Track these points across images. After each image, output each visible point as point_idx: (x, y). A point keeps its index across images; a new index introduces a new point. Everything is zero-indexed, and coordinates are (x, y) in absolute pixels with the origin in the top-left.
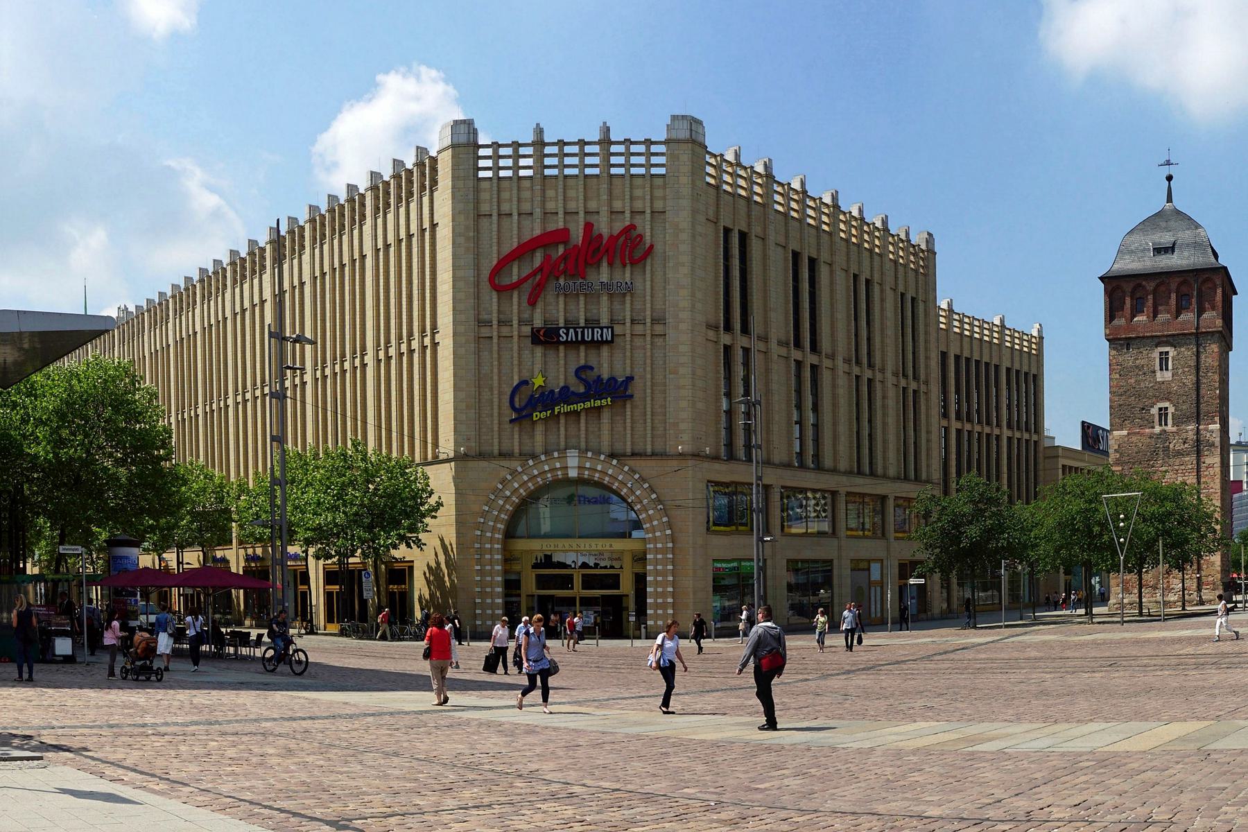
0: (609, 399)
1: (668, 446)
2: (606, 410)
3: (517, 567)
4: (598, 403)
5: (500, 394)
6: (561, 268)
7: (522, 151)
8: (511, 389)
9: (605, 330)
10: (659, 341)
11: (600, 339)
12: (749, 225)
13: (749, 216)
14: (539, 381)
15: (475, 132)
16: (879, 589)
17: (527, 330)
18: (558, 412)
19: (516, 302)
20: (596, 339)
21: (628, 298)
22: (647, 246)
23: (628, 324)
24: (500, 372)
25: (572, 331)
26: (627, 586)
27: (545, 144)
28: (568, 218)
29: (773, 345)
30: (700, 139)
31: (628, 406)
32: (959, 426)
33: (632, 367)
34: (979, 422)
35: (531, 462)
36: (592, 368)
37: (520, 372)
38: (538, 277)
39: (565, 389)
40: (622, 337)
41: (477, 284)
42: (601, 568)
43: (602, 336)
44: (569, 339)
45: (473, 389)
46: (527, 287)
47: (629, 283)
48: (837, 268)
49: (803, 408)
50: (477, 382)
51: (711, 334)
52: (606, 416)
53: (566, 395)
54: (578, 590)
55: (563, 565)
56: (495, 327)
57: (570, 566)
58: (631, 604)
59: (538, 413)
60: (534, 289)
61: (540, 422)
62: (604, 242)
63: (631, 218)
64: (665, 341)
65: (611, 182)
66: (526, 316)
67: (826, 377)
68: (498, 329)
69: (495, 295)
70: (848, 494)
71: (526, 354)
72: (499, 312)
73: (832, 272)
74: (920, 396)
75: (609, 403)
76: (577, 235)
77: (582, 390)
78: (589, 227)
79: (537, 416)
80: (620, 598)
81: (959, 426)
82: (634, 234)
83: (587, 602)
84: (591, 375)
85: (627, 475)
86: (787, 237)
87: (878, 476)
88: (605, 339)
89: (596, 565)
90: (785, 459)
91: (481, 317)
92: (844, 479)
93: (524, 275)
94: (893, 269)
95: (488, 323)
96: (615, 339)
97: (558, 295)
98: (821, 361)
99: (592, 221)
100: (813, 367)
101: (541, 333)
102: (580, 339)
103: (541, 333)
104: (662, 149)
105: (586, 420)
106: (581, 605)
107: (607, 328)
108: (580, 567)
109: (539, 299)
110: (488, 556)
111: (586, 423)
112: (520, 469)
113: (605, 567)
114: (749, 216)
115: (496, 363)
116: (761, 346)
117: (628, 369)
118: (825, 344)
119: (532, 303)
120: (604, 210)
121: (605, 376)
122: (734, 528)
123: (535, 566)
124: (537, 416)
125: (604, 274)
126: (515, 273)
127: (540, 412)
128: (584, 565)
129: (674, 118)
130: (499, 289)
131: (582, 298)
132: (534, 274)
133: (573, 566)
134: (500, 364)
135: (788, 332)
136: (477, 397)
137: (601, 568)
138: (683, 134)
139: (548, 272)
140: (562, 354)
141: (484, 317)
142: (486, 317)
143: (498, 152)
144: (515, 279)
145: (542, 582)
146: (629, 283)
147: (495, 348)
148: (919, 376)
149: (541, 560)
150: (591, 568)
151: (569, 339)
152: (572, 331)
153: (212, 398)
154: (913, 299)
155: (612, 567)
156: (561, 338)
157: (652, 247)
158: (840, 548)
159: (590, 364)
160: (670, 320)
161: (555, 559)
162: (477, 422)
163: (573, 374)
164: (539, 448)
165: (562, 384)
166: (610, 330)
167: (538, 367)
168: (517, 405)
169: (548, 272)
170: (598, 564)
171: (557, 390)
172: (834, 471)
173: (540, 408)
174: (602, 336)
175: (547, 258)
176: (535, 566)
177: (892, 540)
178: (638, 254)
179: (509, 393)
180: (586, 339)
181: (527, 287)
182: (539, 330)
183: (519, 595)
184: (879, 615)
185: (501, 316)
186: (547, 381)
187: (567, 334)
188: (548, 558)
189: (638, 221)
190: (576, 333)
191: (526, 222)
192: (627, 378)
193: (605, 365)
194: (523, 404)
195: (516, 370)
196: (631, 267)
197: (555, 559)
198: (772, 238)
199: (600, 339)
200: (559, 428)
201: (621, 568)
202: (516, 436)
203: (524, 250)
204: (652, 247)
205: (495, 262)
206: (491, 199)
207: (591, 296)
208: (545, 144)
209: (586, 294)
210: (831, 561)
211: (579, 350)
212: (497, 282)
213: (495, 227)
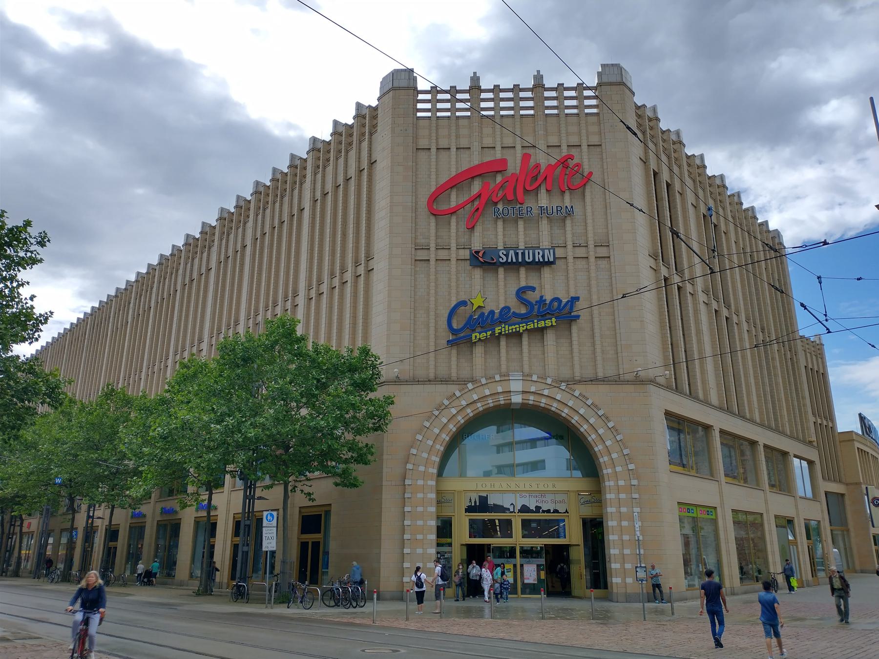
0: (554, 320)
2: (549, 331)
3: (447, 513)
4: (542, 324)
5: (437, 316)
8: (448, 311)
9: (546, 252)
11: (541, 260)
14: (477, 302)
15: (415, 79)
17: (466, 254)
18: (500, 333)
19: (455, 227)
20: (537, 260)
24: (436, 293)
25: (512, 252)
26: (573, 535)
31: (574, 329)
37: (458, 293)
38: (476, 203)
41: (415, 210)
42: (544, 512)
43: (543, 256)
44: (509, 260)
45: (408, 332)
52: (550, 337)
53: (506, 316)
54: (518, 539)
57: (509, 509)
58: (578, 555)
59: (477, 334)
60: (473, 214)
62: (542, 171)
66: (462, 240)
69: (433, 220)
72: (437, 237)
75: (554, 324)
76: (514, 166)
77: (523, 310)
78: (526, 157)
79: (476, 336)
80: (566, 547)
83: (528, 553)
84: (532, 297)
89: (538, 509)
91: (418, 241)
96: (557, 262)
101: (480, 254)
102: (520, 260)
103: (480, 254)
107: (549, 249)
108: (520, 511)
109: (478, 224)
110: (422, 468)
113: (548, 511)
115: (433, 284)
119: (471, 228)
120: (542, 145)
121: (548, 298)
123: (469, 509)
124: (476, 336)
125: (543, 200)
126: (454, 199)
127: (480, 333)
128: (525, 509)
130: (435, 214)
131: (521, 224)
132: (472, 200)
133: (512, 510)
134: (436, 287)
136: (412, 318)
137: (544, 512)
140: (501, 283)
141: (421, 241)
142: (423, 241)
144: (453, 204)
145: (479, 528)
147: (433, 270)
149: (475, 502)
150: (532, 511)
151: (509, 260)
152: (512, 252)
153: (154, 362)
155: (556, 511)
156: (501, 260)
157: (591, 174)
161: (491, 502)
164: (478, 372)
165: (502, 305)
166: (552, 251)
168: (455, 326)
170: (540, 508)
171: (497, 311)
174: (543, 256)
175: (486, 186)
176: (469, 509)
177: (798, 498)
179: (447, 315)
180: (527, 259)
182: (477, 252)
183: (450, 545)
185: (439, 241)
188: (484, 500)
190: (517, 254)
191: (465, 155)
194: (460, 326)
195: (454, 291)
196: (571, 194)
199: (541, 260)
201: (566, 512)
205: (433, 189)
206: (430, 135)
207: (531, 220)
211: (453, 492)
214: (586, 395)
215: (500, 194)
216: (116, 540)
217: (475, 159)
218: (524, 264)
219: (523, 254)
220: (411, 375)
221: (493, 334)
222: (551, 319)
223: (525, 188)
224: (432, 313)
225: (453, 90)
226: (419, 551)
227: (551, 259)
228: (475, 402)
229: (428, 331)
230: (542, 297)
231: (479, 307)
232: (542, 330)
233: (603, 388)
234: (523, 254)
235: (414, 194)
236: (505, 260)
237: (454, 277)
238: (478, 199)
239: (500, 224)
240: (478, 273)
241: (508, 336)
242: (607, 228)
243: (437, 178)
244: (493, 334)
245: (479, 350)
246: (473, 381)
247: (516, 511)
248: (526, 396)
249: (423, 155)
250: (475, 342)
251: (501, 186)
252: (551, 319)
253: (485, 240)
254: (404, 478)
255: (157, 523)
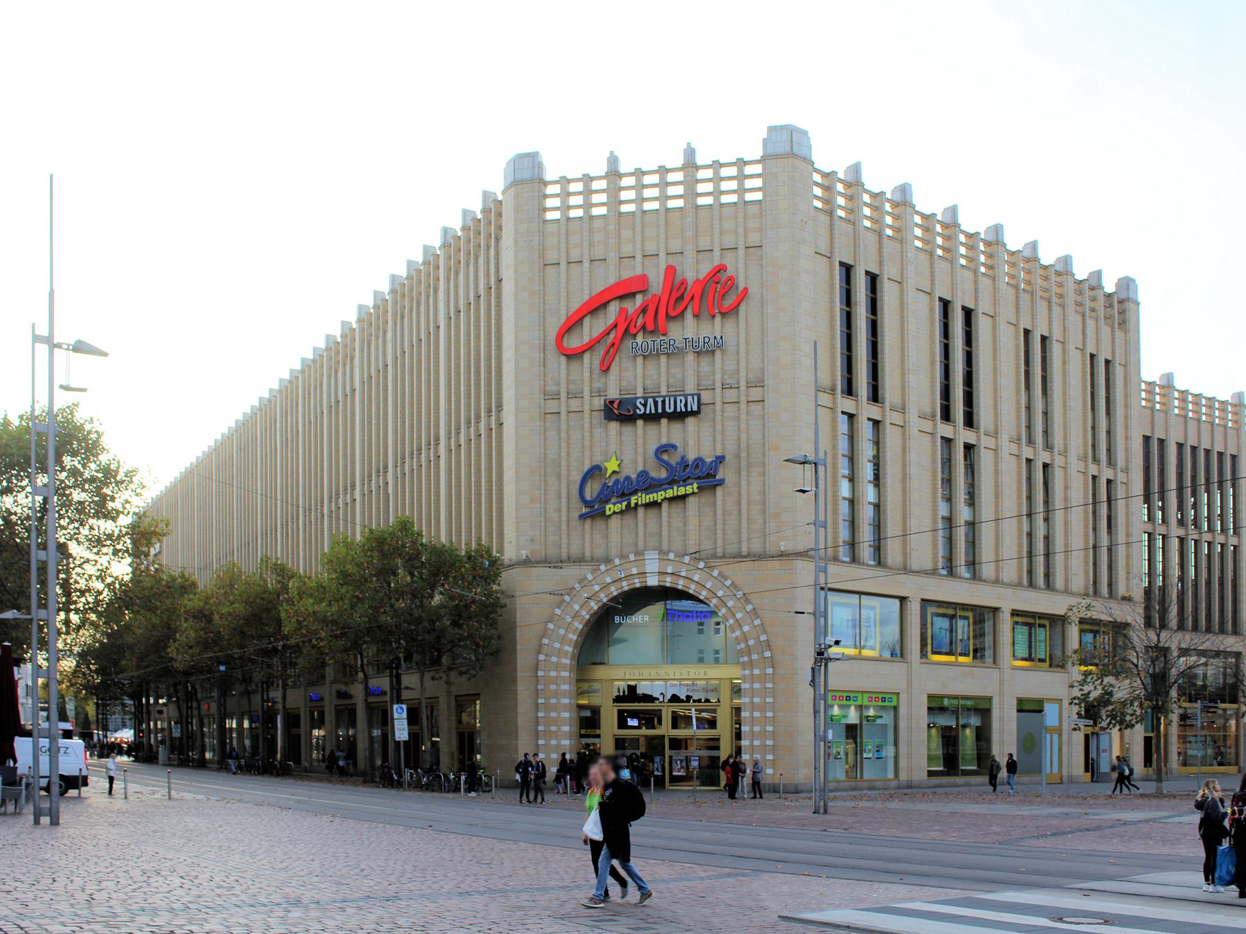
0: (695, 485)
1: (767, 544)
3: (595, 700)
4: (682, 491)
6: (639, 323)
7: (749, 170)
9: (690, 398)
10: (756, 409)
11: (684, 410)
12: (881, 264)
13: (880, 253)
14: (612, 466)
16: (1056, 737)
17: (599, 403)
20: (678, 410)
21: (718, 354)
22: (741, 289)
23: (718, 390)
25: (650, 401)
27: (698, 168)
28: (647, 261)
29: (913, 417)
30: (804, 153)
32: (1181, 532)
33: (723, 444)
34: (1222, 530)
35: (603, 568)
36: (674, 447)
38: (612, 336)
39: (643, 474)
40: (712, 406)
42: (694, 701)
43: (686, 405)
44: (648, 412)
46: (600, 350)
47: (718, 337)
48: (1001, 322)
49: (953, 500)
50: (542, 469)
51: (825, 399)
52: (691, 501)
55: (649, 698)
56: (563, 399)
57: (658, 699)
59: (611, 506)
61: (614, 517)
62: (689, 288)
63: (721, 257)
64: (763, 409)
65: (697, 214)
66: (597, 385)
67: (985, 460)
68: (567, 402)
69: (563, 359)
70: (1015, 613)
71: (598, 432)
73: (994, 327)
74: (1116, 487)
75: (696, 490)
76: (657, 284)
78: (671, 270)
81: (1181, 532)
82: (724, 277)
85: (738, 603)
86: (932, 282)
87: (1057, 591)
88: (689, 409)
90: (928, 565)
91: (548, 388)
92: (1009, 591)
93: (595, 334)
94: (1080, 325)
95: (556, 396)
97: (635, 357)
98: (978, 439)
99: (674, 264)
100: (968, 448)
101: (615, 405)
102: (660, 410)
103: (615, 405)
104: (758, 169)
105: (669, 513)
106: (671, 748)
107: (693, 395)
108: (671, 700)
109: (614, 363)
110: (554, 659)
111: (669, 517)
112: (590, 577)
114: (880, 253)
116: (897, 418)
117: (719, 446)
118: (1120, 462)
119: (606, 369)
120: (690, 250)
121: (691, 457)
122: (952, 658)
123: (618, 699)
127: (614, 504)
128: (675, 699)
129: (772, 130)
134: (568, 447)
135: (933, 401)
137: (694, 701)
138: (783, 148)
139: (625, 328)
141: (551, 388)
143: (743, 171)
144: (586, 339)
146: (718, 337)
148: (1116, 461)
150: (682, 701)
151: (648, 412)
152: (650, 401)
154: (1044, 339)
156: (638, 411)
157: (746, 290)
158: (1001, 683)
159: (674, 442)
160: (769, 382)
161: (640, 691)
162: (543, 519)
163: (653, 456)
165: (640, 468)
166: (696, 397)
167: (613, 447)
168: (588, 497)
169: (625, 328)
170: (691, 697)
172: (906, 570)
173: (613, 500)
174: (686, 405)
175: (623, 311)
178: (728, 302)
179: (579, 482)
180: (667, 410)
181: (600, 350)
182: (612, 402)
184: (1056, 770)
185: (572, 387)
186: (623, 465)
187: (645, 405)
188: (632, 689)
189: (729, 260)
190: (656, 403)
192: (717, 457)
193: (691, 443)
194: (595, 495)
195: (587, 453)
197: (640, 691)
198: (911, 282)
199: (684, 410)
200: (637, 524)
201: (719, 701)
202: (587, 536)
203: (596, 306)
204: (746, 290)
208: (698, 168)
209: (1206, 741)
210: (990, 699)
212: (565, 345)
213: (563, 277)
214: (727, 573)
215: (640, 322)
216: (299, 726)
217: (607, 278)
218: (665, 414)
219: (663, 402)
220: (543, 556)
221: (629, 504)
222: (692, 484)
223: (667, 313)
224: (564, 481)
225: (563, 180)
226: (554, 742)
227: (695, 408)
228: (620, 580)
229: (560, 502)
230: (683, 457)
231: (614, 472)
232: (684, 497)
233: (747, 565)
234: (663, 402)
235: (542, 328)
236: (642, 412)
237: (587, 434)
238: (614, 331)
239: (640, 360)
240: (614, 426)
241: (672, 500)
242: (763, 362)
243: (568, 302)
244: (628, 506)
245: (615, 522)
246: (607, 560)
247: (666, 700)
248: (663, 577)
249: (551, 271)
250: (610, 516)
251: (644, 310)
252: (692, 484)
253: (624, 383)
254: (537, 669)
255: (456, 700)
